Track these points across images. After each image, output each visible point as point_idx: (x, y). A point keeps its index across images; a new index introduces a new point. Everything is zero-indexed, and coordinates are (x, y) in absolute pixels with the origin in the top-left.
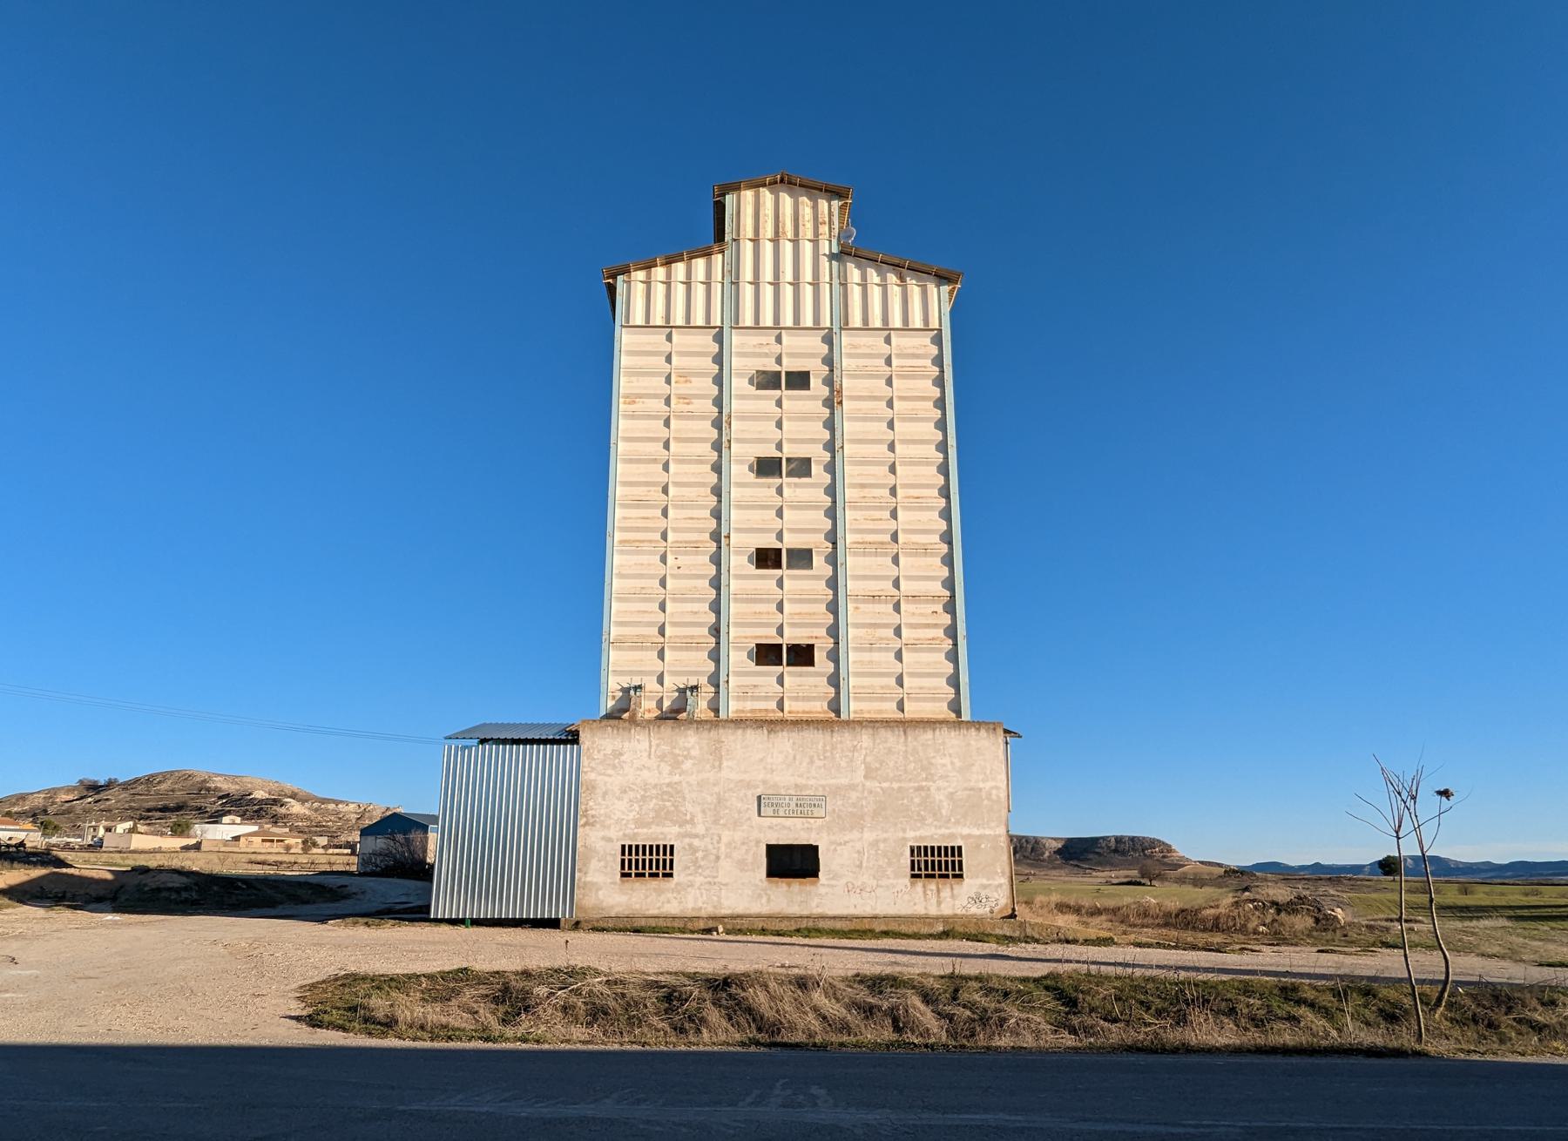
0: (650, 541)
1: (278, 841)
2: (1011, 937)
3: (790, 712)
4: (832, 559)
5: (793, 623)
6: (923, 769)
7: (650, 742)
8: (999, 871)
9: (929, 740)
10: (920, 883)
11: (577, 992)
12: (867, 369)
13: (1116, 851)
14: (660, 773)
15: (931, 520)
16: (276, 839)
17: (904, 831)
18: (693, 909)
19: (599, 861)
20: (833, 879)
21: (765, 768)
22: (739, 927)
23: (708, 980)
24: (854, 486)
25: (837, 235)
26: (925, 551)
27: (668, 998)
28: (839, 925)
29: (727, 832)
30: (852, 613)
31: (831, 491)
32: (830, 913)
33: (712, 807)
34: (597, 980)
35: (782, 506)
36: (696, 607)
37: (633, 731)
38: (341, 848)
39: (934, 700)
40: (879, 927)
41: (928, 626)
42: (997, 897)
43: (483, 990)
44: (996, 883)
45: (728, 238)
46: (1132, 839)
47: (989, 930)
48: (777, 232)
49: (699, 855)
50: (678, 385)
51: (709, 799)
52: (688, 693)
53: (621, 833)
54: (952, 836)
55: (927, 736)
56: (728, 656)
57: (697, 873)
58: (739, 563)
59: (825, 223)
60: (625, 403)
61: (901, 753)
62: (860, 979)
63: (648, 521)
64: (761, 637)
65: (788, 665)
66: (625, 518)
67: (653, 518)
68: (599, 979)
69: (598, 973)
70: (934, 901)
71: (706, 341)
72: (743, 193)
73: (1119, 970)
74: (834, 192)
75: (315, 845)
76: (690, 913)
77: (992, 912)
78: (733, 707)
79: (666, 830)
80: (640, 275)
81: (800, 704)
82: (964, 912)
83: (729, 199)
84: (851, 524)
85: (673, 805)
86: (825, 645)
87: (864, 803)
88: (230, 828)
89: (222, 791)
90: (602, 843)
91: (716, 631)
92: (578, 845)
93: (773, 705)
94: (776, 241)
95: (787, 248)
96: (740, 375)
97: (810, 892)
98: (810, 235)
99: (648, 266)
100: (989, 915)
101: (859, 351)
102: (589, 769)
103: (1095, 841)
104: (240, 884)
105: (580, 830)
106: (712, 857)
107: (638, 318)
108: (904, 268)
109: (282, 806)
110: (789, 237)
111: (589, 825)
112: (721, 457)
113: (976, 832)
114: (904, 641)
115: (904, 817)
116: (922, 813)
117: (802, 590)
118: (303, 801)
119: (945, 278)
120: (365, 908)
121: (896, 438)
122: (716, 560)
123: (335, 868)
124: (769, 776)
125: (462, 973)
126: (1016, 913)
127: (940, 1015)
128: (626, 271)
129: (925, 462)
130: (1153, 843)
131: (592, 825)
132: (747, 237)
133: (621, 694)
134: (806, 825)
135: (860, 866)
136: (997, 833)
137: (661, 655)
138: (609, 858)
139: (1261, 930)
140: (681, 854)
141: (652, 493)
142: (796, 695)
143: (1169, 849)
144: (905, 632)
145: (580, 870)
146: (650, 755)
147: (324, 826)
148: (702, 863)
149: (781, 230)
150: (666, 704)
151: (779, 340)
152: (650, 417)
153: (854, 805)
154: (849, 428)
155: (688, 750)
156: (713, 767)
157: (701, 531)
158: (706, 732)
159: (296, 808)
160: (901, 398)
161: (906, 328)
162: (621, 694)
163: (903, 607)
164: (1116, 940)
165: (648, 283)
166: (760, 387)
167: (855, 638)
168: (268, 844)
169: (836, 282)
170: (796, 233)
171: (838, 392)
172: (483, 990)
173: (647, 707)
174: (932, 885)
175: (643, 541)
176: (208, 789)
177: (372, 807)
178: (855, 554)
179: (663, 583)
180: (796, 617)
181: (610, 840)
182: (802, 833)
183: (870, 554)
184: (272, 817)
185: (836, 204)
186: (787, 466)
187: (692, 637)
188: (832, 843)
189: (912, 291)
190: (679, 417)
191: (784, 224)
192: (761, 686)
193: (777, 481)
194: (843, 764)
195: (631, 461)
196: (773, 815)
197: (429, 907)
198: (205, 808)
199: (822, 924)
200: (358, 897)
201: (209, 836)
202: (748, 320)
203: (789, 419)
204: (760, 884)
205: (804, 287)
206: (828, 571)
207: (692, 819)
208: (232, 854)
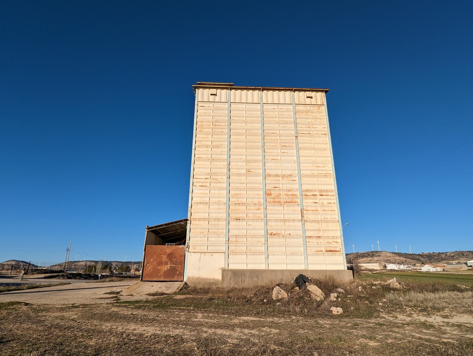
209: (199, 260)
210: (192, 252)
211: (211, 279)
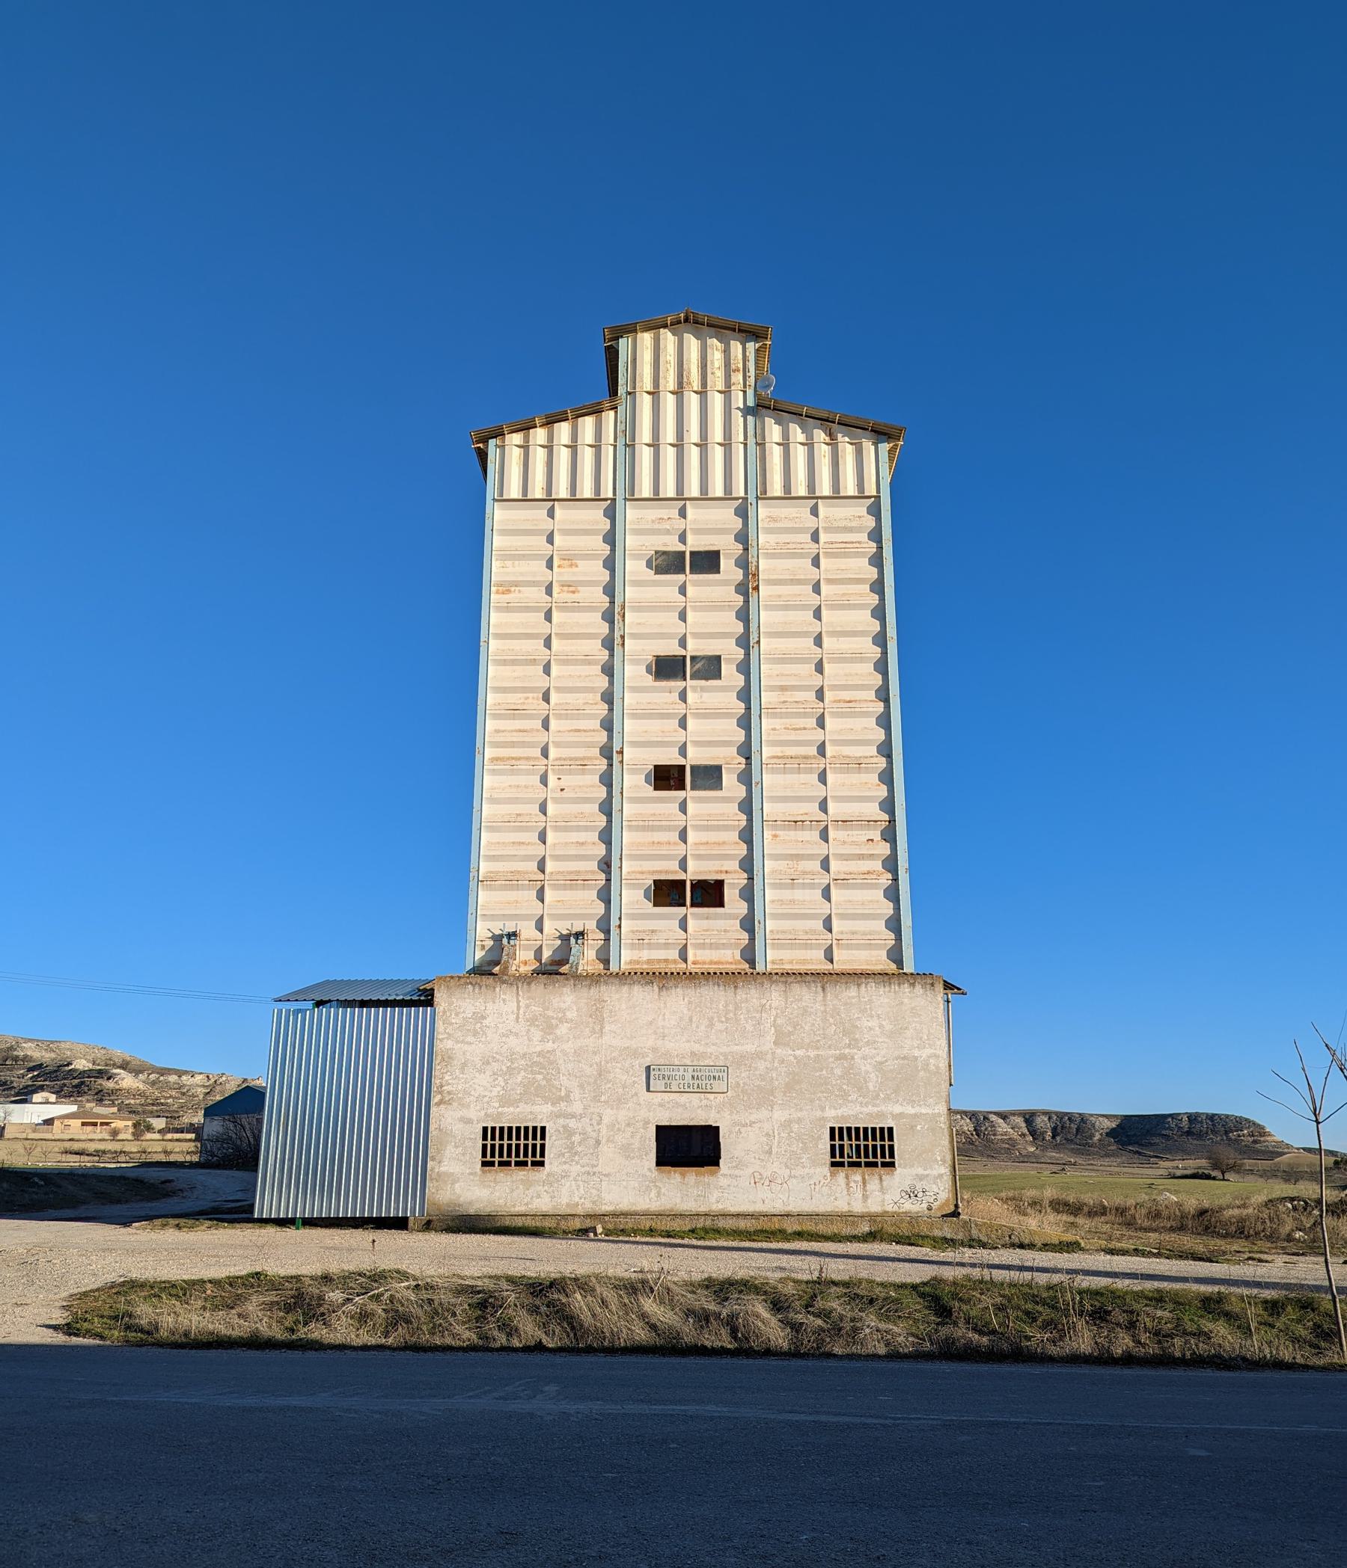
0: (528, 759)
1: (102, 1124)
2: (952, 1240)
3: (694, 963)
4: (746, 778)
5: (699, 855)
6: (845, 1033)
7: (518, 1002)
8: (939, 1159)
9: (853, 997)
10: (841, 1173)
11: (377, 1298)
12: (789, 546)
13: (1189, 1133)
14: (529, 1040)
15: (866, 728)
16: (99, 1121)
17: (823, 1109)
18: (568, 1205)
19: (456, 1147)
20: (736, 1167)
21: (655, 1033)
22: (622, 1227)
23: (532, 1285)
24: (772, 688)
25: (753, 385)
26: (859, 765)
27: (483, 1305)
28: (742, 1224)
29: (609, 1110)
30: (768, 841)
31: (745, 695)
32: (733, 1209)
33: (592, 1080)
34: (403, 1285)
35: (685, 715)
36: (582, 836)
37: (498, 989)
38: (182, 1132)
39: (870, 947)
40: (791, 1226)
41: (861, 857)
42: (936, 1190)
43: (272, 1297)
44: (935, 1173)
45: (621, 390)
46: (1212, 1117)
47: (925, 1231)
48: (680, 384)
49: (576, 1138)
50: (561, 570)
51: (588, 1071)
52: (573, 940)
53: (483, 1113)
54: (881, 1115)
55: (850, 992)
56: (621, 895)
57: (572, 1161)
58: (634, 782)
59: (738, 371)
60: (497, 592)
61: (819, 1014)
62: (708, 1284)
63: (525, 734)
64: (661, 872)
65: (693, 905)
66: (497, 731)
67: (532, 730)
68: (407, 1284)
69: (403, 1275)
70: (859, 1195)
71: (595, 516)
72: (639, 335)
73: (1014, 1275)
74: (750, 332)
75: (149, 1128)
76: (564, 1210)
77: (930, 1209)
78: (626, 957)
79: (536, 1109)
80: (517, 438)
81: (707, 952)
82: (896, 1209)
83: (624, 345)
84: (769, 734)
85: (544, 1078)
86: (736, 881)
87: (774, 1075)
88: (42, 1108)
89: (34, 1061)
90: (461, 1126)
91: (606, 865)
92: (432, 1127)
93: (674, 954)
94: (678, 393)
95: (693, 401)
96: (637, 557)
97: (709, 1184)
98: (721, 386)
99: (527, 427)
100: (927, 1212)
101: (779, 525)
102: (446, 1036)
103: (1161, 1119)
104: (36, 1180)
105: (433, 1110)
106: (592, 1142)
107: (514, 490)
108: (834, 422)
109: (109, 1079)
110: (695, 389)
111: (445, 1103)
112: (613, 655)
113: (910, 1110)
114: (833, 876)
115: (823, 1092)
116: (845, 1087)
117: (709, 815)
118: (136, 1072)
119: (885, 434)
120: (188, 1205)
121: (824, 630)
122: (607, 780)
123: (172, 1158)
124: (660, 1042)
125: (253, 1278)
126: (960, 1210)
127: (786, 1323)
128: (499, 434)
129: (857, 658)
130: (1240, 1123)
131: (449, 1103)
132: (645, 390)
133: (492, 943)
134: (705, 1102)
135: (770, 1153)
136: (937, 1111)
137: (541, 897)
138: (468, 1144)
139: (1297, 1236)
140: (554, 1138)
141: (530, 701)
142: (702, 941)
143: (1259, 1131)
144: (834, 865)
145: (433, 1159)
146: (517, 1018)
147: (162, 1104)
148: (580, 1149)
149: (685, 380)
150: (546, 954)
151: (683, 513)
152: (527, 609)
153: (762, 1077)
154: (766, 618)
155: (564, 1011)
156: (593, 1032)
157: (588, 745)
158: (585, 990)
159: (127, 1081)
160: (830, 581)
161: (836, 496)
162: (492, 943)
163: (832, 834)
164: (1083, 1245)
165: (525, 447)
166: (660, 570)
167: (773, 872)
168: (90, 1128)
169: (751, 441)
170: (704, 383)
171: (754, 575)
172: (272, 1297)
173: (523, 959)
174: (857, 1175)
175: (519, 759)
176: (16, 1059)
177: (224, 1079)
178: (774, 771)
179: (543, 809)
180: (702, 847)
181: (469, 1121)
182: (699, 1111)
183: (792, 771)
184: (97, 1094)
185: (751, 346)
186: (692, 667)
187: (578, 872)
188: (735, 1124)
189: (844, 450)
190: (563, 609)
191: (689, 373)
192: (660, 931)
193: (681, 684)
194: (749, 1028)
195: (504, 663)
196: (664, 1090)
197: (252, 1206)
198: (12, 1082)
199: (722, 1224)
200: (185, 1194)
201: (14, 1119)
202: (645, 489)
203: (695, 609)
204: (648, 1174)
205: (713, 448)
206: (741, 792)
207: (568, 1096)
208: (40, 1142)
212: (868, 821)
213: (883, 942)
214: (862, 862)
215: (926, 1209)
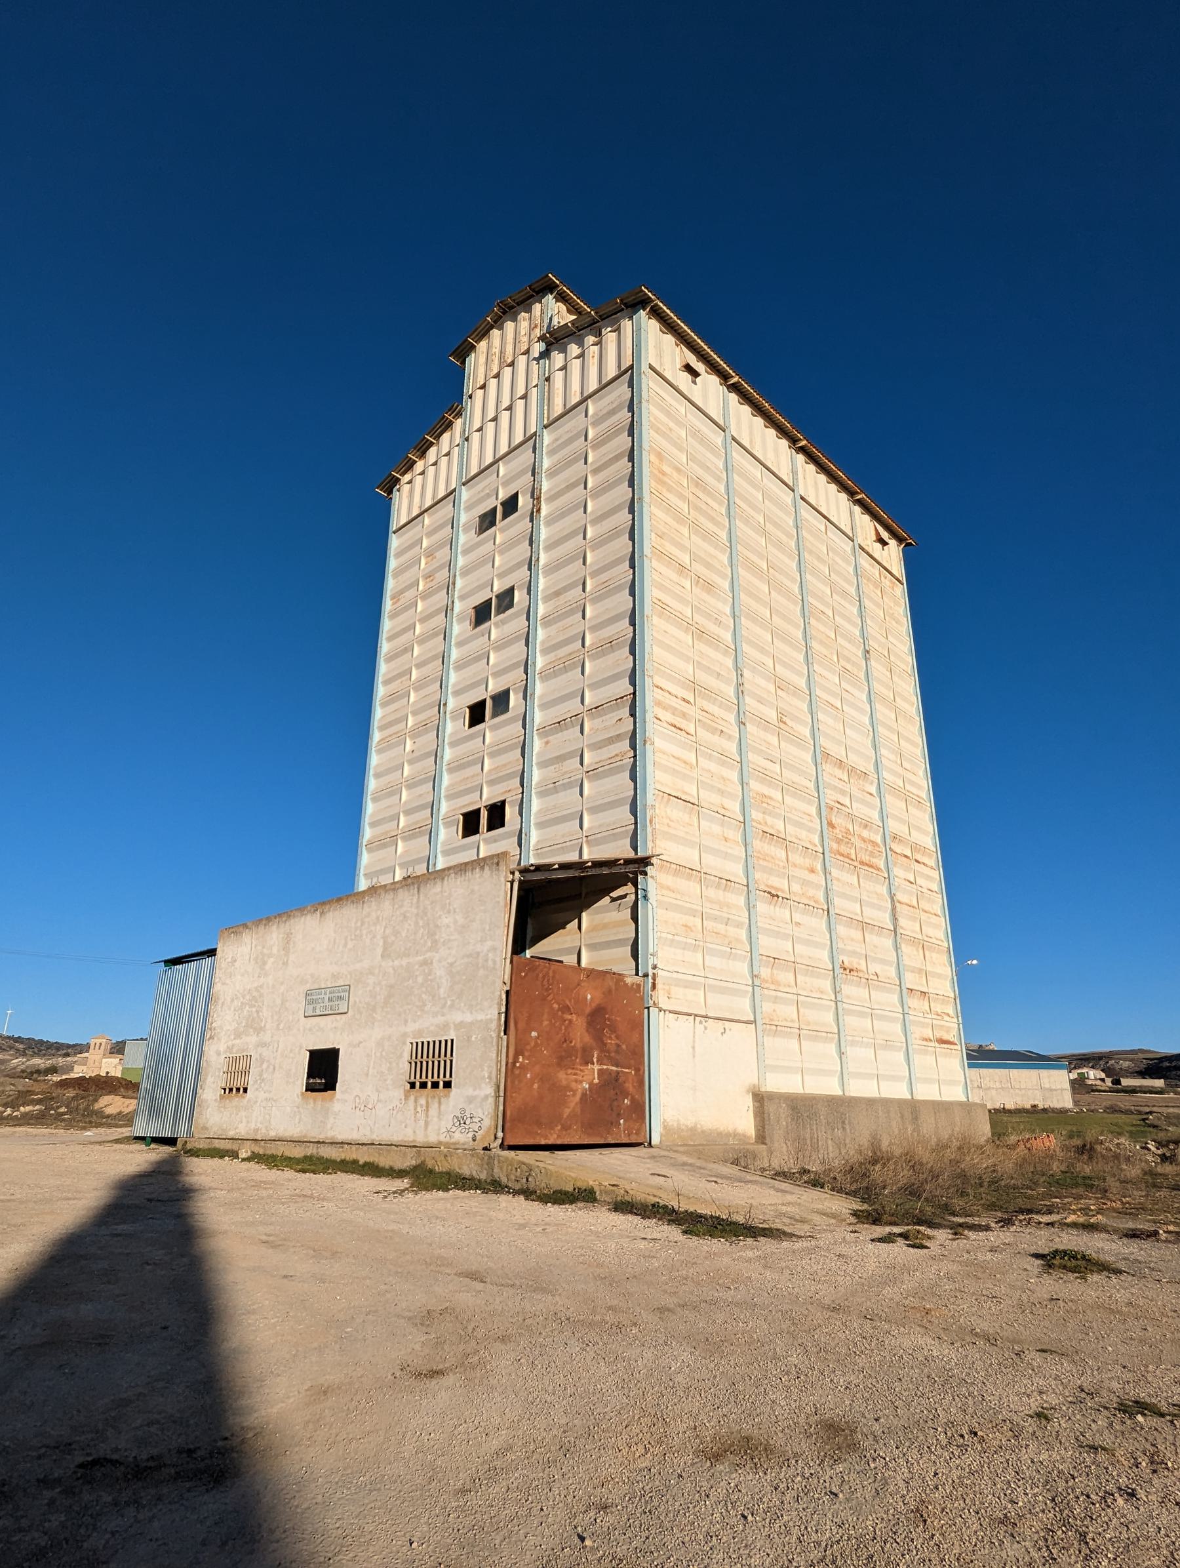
64: (464, 806)
82: (448, 1139)
100: (471, 1143)
113: (468, 1018)
209: (691, 1050)
210: (670, 1012)
211: (728, 1135)
212: (616, 700)
213: (624, 829)
214: (613, 746)
215: (471, 1139)
